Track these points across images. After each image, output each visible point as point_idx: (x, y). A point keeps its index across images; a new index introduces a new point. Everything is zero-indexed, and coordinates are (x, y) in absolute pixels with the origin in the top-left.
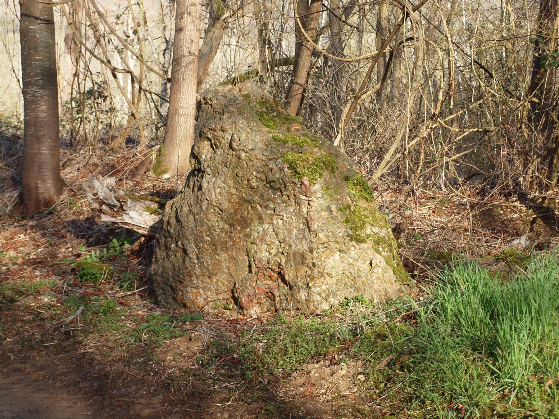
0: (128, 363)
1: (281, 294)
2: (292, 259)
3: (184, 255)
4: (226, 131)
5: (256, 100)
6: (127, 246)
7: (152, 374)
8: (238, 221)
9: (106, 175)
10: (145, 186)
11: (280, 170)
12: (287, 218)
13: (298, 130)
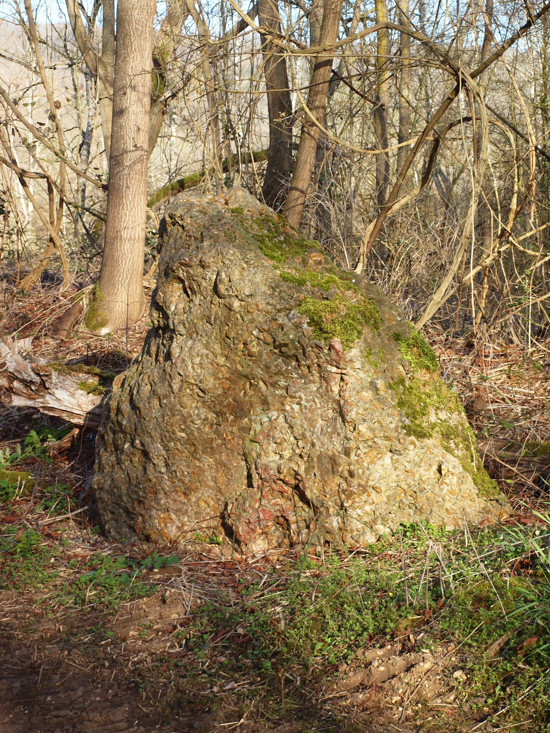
0: (65, 641)
1: (299, 519)
2: (316, 465)
3: (144, 459)
4: (209, 267)
5: (252, 216)
6: (52, 442)
7: (107, 664)
8: (231, 408)
9: (15, 330)
10: (74, 347)
11: (294, 326)
12: (307, 401)
13: (320, 263)
